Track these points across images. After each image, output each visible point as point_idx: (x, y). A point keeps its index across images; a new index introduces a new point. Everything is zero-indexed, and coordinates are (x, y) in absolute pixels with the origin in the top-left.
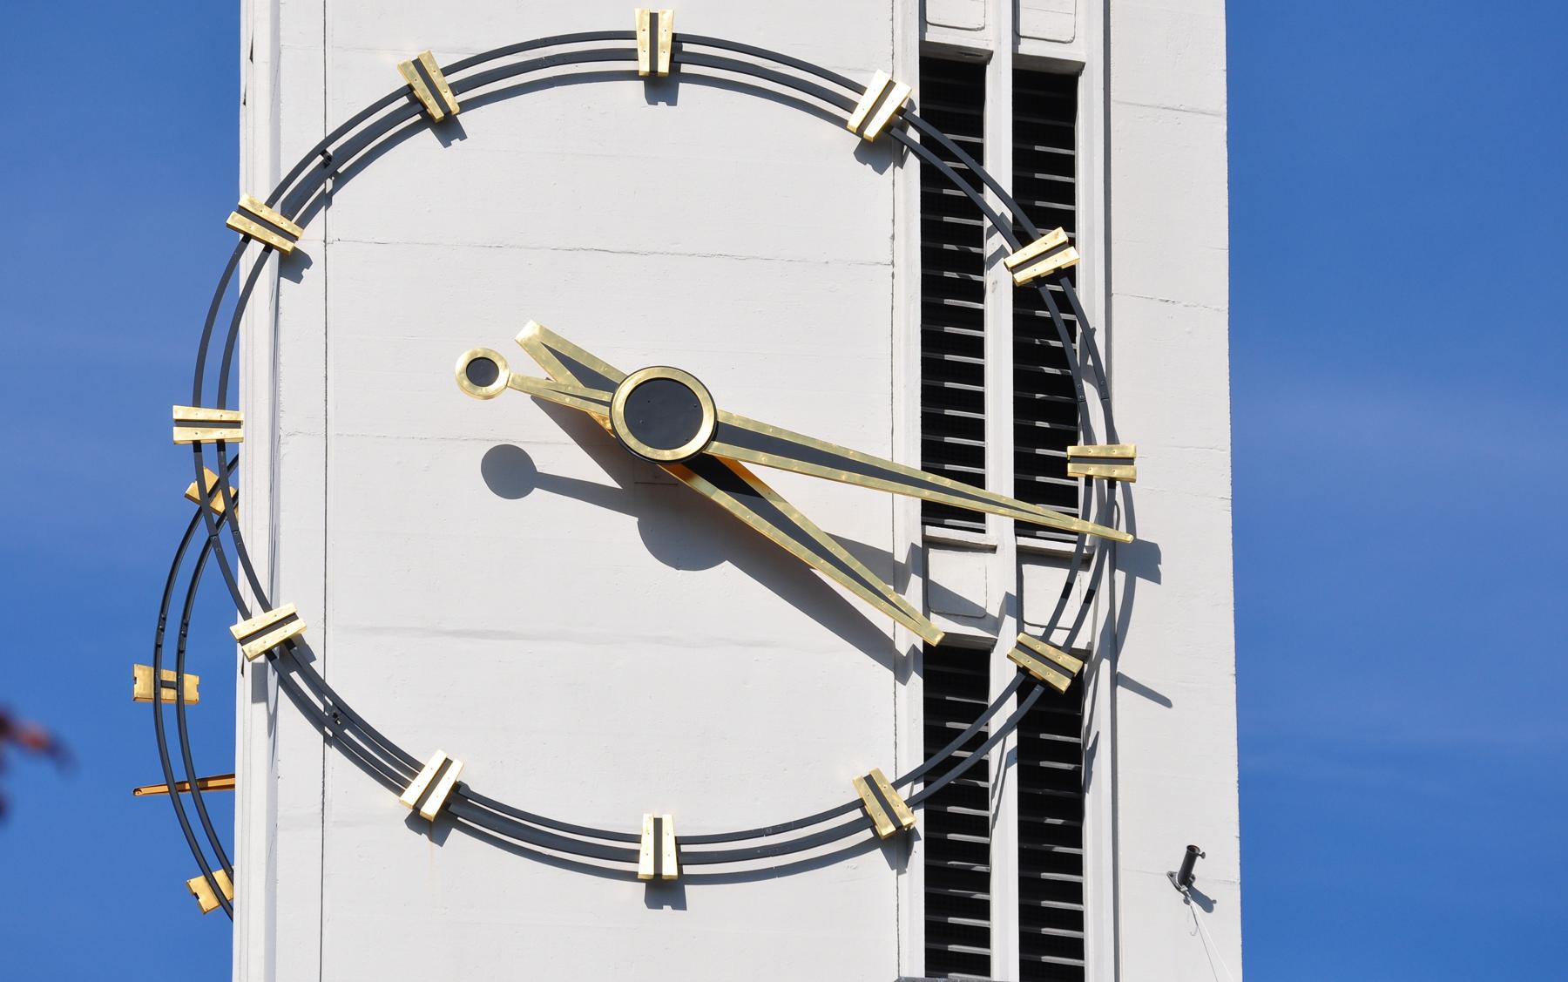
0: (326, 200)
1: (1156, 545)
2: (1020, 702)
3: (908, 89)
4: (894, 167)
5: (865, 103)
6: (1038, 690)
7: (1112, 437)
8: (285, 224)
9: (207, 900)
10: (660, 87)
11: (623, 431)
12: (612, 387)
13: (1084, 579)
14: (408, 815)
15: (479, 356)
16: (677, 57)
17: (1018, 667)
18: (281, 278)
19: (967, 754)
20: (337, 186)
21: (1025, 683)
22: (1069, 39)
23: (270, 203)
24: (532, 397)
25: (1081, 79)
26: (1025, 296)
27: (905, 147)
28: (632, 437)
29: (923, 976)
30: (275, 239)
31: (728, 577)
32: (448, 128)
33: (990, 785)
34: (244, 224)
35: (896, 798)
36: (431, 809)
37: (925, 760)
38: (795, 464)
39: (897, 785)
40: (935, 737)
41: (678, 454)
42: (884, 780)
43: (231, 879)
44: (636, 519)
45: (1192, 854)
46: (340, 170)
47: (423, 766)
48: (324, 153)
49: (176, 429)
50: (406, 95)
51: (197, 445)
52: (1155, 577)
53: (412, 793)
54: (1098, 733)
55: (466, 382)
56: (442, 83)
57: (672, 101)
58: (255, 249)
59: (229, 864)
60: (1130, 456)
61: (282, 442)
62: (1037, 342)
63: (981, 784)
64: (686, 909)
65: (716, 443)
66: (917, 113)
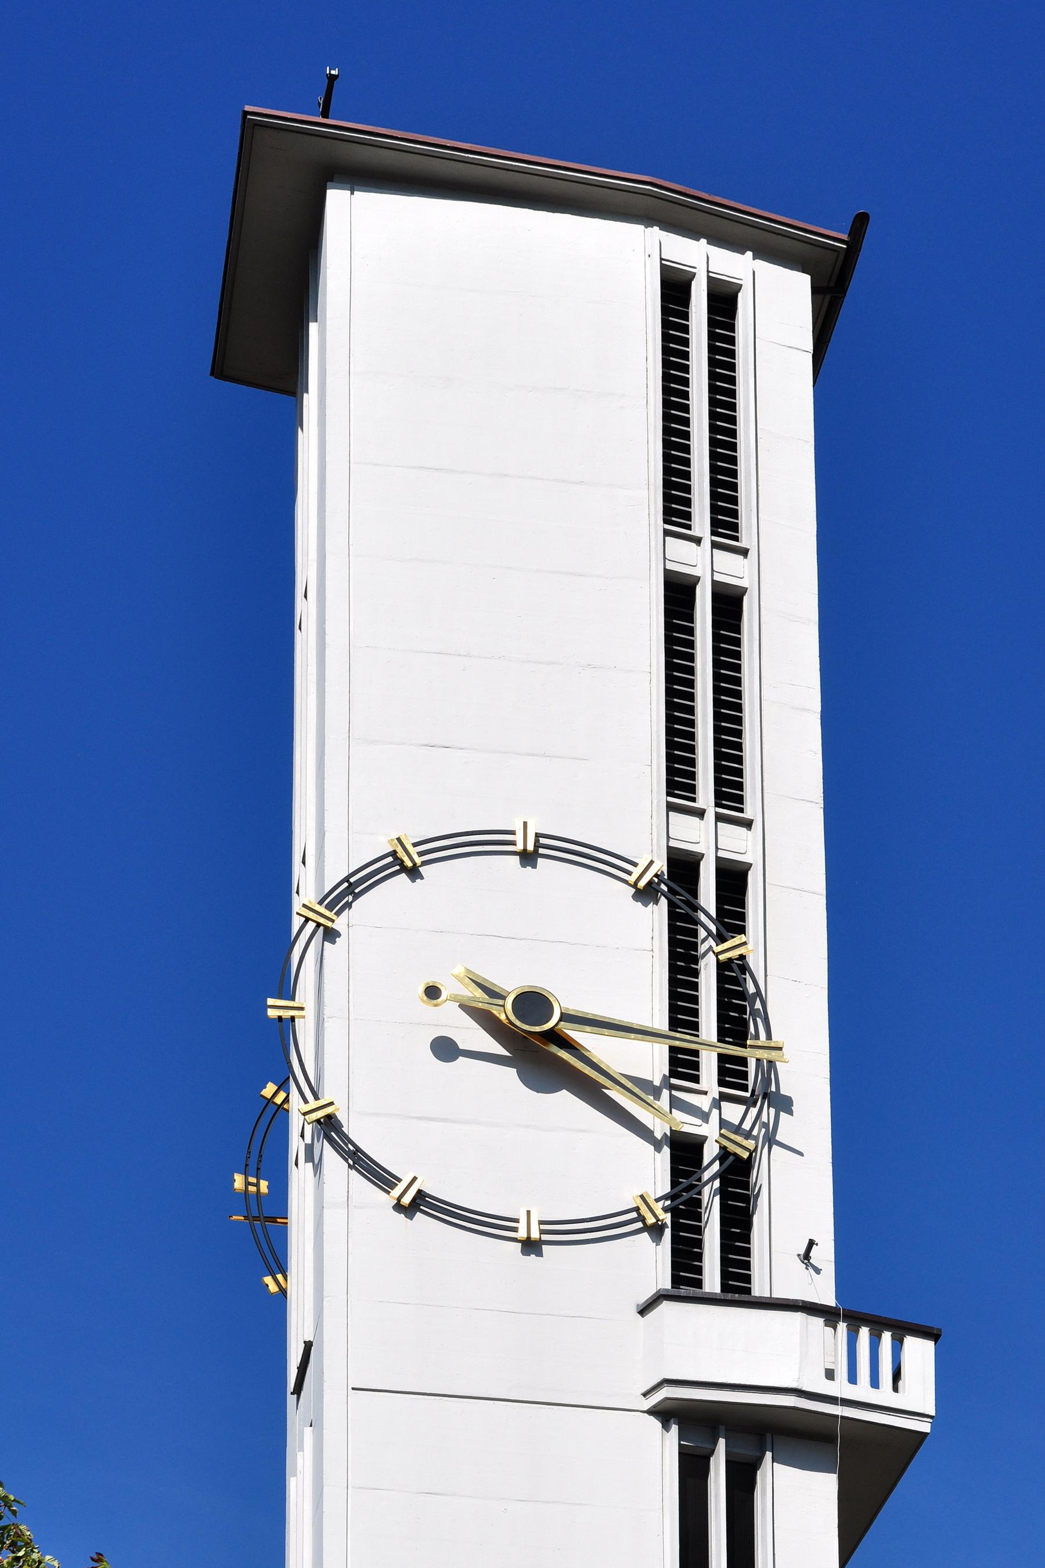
0: (349, 905)
1: (790, 1097)
2: (721, 1165)
3: (661, 865)
4: (653, 904)
5: (637, 872)
6: (732, 1158)
7: (769, 1036)
8: (327, 913)
9: (273, 1288)
10: (528, 858)
11: (513, 1018)
12: (504, 998)
13: (754, 1111)
14: (394, 1204)
15: (431, 985)
16: (538, 844)
17: (720, 1146)
18: (325, 942)
19: (694, 1182)
20: (354, 900)
21: (724, 1155)
22: (744, 852)
23: (321, 903)
24: (459, 1006)
25: (750, 873)
26: (723, 967)
27: (659, 894)
28: (517, 1020)
29: (670, 1287)
30: (322, 920)
31: (565, 1099)
32: (414, 873)
33: (703, 1211)
34: (306, 912)
35: (656, 1207)
36: (406, 1200)
37: (671, 1189)
38: (606, 1031)
39: (657, 1200)
40: (676, 1174)
41: (543, 1028)
42: (649, 1197)
43: (286, 1280)
44: (515, 1070)
45: (811, 1243)
46: (357, 891)
47: (402, 1180)
48: (348, 881)
49: (269, 1010)
50: (392, 856)
51: (280, 1018)
52: (791, 1113)
53: (396, 1192)
54: (761, 1185)
55: (425, 998)
56: (413, 851)
57: (534, 866)
58: (311, 926)
59: (284, 1271)
60: (781, 1046)
61: (325, 1021)
62: (726, 1000)
63: (699, 1210)
64: (542, 1257)
65: (562, 1023)
66: (666, 877)
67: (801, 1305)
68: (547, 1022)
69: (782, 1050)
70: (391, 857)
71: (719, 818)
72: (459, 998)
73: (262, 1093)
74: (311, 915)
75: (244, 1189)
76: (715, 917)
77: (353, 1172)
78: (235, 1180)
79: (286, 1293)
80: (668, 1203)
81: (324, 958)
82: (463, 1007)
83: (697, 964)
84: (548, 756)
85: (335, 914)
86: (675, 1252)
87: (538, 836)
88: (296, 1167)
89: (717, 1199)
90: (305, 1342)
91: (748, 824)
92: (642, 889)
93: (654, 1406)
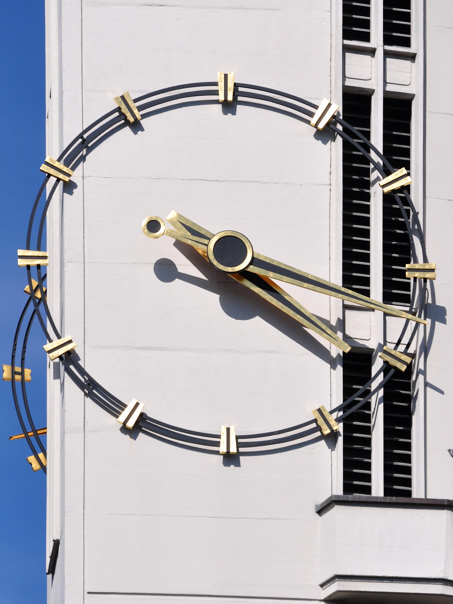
0: (83, 158)
5: (318, 113)
6: (392, 371)
7: (425, 260)
8: (65, 169)
9: (36, 466)
12: (209, 239)
15: (153, 219)
16: (236, 93)
18: (64, 193)
20: (88, 152)
22: (408, 84)
27: (336, 133)
30: (61, 176)
34: (48, 169)
36: (131, 424)
37: (343, 401)
39: (331, 412)
46: (89, 145)
48: (82, 137)
49: (19, 260)
51: (28, 267)
54: (418, 389)
55: (146, 230)
56: (134, 106)
57: (234, 113)
60: (433, 268)
61: (65, 265)
62: (393, 219)
65: (252, 266)
66: (341, 117)
67: (446, 504)
68: (240, 264)
69: (434, 272)
70: (117, 113)
71: (387, 54)
72: (174, 233)
73: (25, 290)
74: (52, 171)
75: (11, 378)
76: (382, 153)
77: (88, 400)
80: (341, 413)
81: (64, 208)
83: (369, 189)
84: (246, 9)
86: (346, 451)
89: (381, 406)
90: (54, 540)
91: (412, 57)
92: (321, 130)
93: (329, 596)
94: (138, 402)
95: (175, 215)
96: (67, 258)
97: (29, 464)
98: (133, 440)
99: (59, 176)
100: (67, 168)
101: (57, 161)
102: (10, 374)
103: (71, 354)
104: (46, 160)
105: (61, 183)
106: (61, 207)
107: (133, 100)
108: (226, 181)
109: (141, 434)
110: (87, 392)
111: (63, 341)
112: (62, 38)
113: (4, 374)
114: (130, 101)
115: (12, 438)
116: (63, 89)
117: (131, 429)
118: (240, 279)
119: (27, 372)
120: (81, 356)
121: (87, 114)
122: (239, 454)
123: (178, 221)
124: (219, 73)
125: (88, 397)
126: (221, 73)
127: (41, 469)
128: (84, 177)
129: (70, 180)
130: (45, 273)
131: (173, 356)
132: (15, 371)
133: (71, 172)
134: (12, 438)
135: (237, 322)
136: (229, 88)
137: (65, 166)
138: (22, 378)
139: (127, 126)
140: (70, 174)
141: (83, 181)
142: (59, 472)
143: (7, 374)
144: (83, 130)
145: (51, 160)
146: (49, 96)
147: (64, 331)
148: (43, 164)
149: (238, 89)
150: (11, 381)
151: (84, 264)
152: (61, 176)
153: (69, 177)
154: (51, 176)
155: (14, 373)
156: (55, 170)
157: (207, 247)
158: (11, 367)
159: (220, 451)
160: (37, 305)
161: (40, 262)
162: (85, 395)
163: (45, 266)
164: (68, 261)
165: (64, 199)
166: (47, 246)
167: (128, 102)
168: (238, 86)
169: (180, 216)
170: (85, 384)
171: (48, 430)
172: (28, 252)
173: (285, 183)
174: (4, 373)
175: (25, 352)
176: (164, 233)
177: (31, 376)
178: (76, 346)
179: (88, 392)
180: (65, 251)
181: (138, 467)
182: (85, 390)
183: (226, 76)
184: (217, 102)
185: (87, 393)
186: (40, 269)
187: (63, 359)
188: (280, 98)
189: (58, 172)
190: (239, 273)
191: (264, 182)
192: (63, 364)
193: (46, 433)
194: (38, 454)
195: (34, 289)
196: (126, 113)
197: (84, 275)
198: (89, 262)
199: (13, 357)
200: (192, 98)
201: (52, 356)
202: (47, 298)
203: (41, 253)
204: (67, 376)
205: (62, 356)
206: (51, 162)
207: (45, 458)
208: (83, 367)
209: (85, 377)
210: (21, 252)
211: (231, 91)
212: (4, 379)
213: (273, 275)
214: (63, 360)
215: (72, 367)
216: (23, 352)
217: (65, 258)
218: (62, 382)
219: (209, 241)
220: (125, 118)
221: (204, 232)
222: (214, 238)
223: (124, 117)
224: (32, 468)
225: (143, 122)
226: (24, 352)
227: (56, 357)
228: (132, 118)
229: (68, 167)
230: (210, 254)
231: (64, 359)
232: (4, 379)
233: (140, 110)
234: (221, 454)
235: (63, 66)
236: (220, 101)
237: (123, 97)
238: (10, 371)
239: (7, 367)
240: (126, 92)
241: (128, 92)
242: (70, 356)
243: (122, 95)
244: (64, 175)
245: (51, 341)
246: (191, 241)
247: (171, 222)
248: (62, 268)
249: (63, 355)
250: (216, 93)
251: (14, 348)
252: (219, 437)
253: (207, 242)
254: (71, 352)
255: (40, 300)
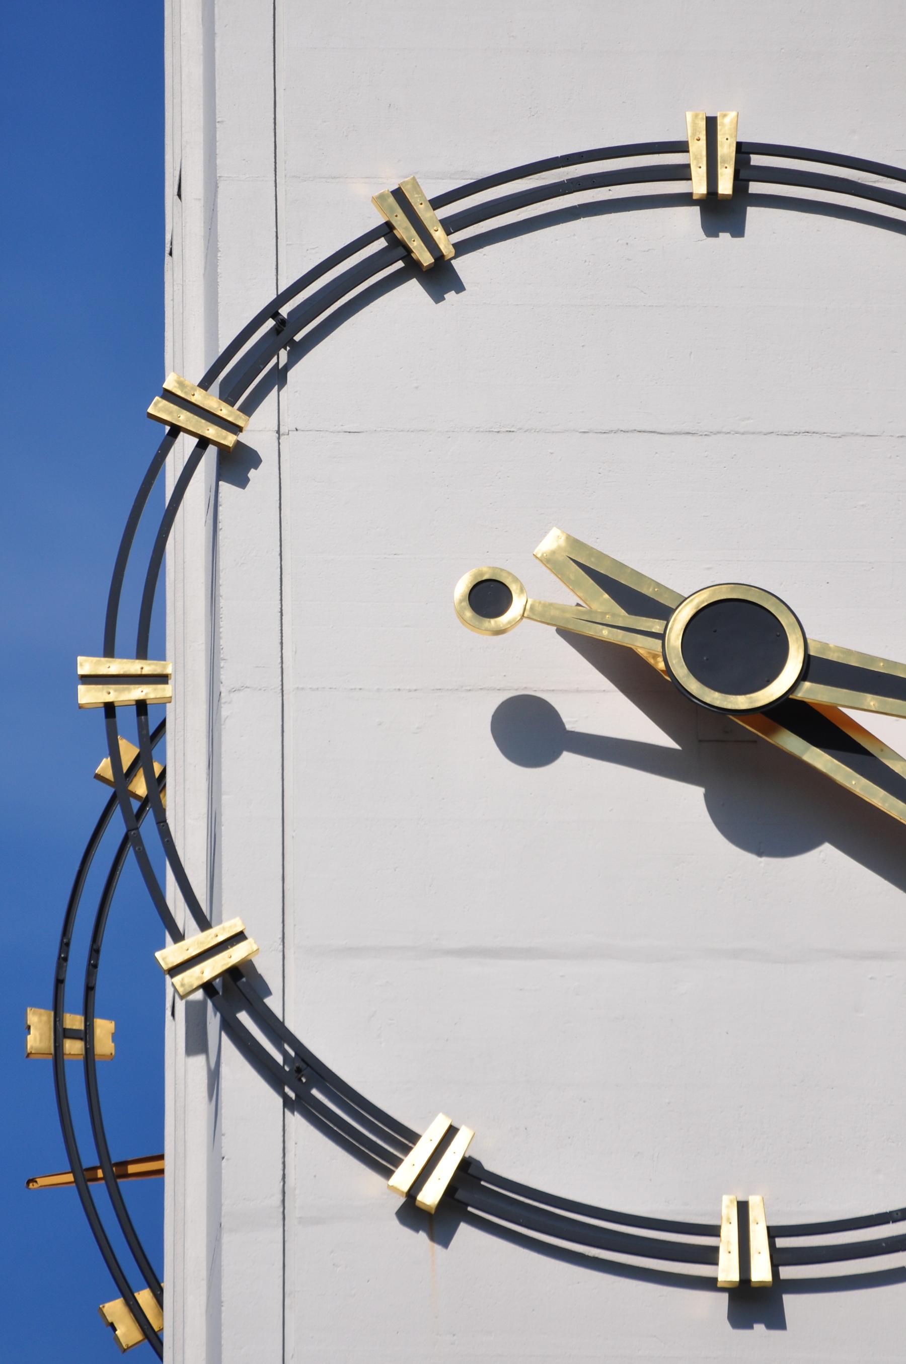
0: (279, 377)
8: (225, 411)
12: (664, 613)
15: (486, 577)
18: (221, 483)
20: (294, 358)
30: (211, 431)
34: (171, 413)
46: (298, 337)
48: (275, 315)
49: (82, 689)
51: (110, 709)
53: (404, 1177)
55: (469, 613)
56: (432, 218)
57: (738, 231)
58: (185, 445)
61: (223, 700)
65: (807, 685)
72: (553, 612)
73: (96, 772)
74: (183, 418)
77: (296, 1121)
78: (29, 1028)
79: (161, 1343)
81: (220, 526)
82: (566, 634)
85: (240, 409)
87: (743, 150)
88: (172, 1018)
94: (453, 1124)
95: (562, 541)
96: (228, 676)
97: (107, 1326)
98: (438, 1248)
99: (207, 432)
100: (230, 408)
101: (198, 388)
102: (50, 1037)
103: (242, 976)
104: (165, 386)
105: (211, 453)
106: (211, 522)
107: (431, 201)
108: (719, 433)
109: (464, 1229)
110: (292, 1095)
111: (217, 936)
112: (216, 27)
113: (29, 1037)
114: (421, 204)
115: (34, 1184)
116: (218, 175)
117: (433, 1212)
118: (770, 732)
119: (104, 1029)
120: (273, 982)
121: (290, 245)
122: (779, 1286)
123: (569, 557)
124: (689, 116)
125: (296, 1113)
126: (696, 116)
127: (146, 1341)
128: (281, 432)
129: (238, 444)
130: (163, 719)
131: (562, 976)
132: (64, 1027)
133: (240, 418)
134: (36, 1182)
135: (762, 865)
136: (721, 157)
137: (224, 401)
138: (86, 1049)
139: (412, 279)
140: (240, 423)
141: (279, 444)
142: (204, 1355)
143: (38, 1039)
144: (279, 293)
145: (181, 384)
146: (176, 193)
147: (221, 905)
148: (157, 398)
149: (749, 160)
150: (51, 1058)
151: (280, 695)
152: (211, 431)
153: (235, 433)
154: (182, 433)
155: (61, 1033)
156: (192, 415)
157: (660, 642)
158: (52, 1013)
159: (719, 1279)
160: (134, 819)
161: (146, 694)
162: (285, 1105)
163: (162, 705)
164: (232, 686)
165: (220, 499)
166: (168, 638)
167: (415, 208)
168: (748, 151)
169: (574, 543)
170: (287, 1069)
171: (168, 1164)
172: (110, 662)
173: (901, 435)
174: (29, 1033)
175: (95, 966)
176: (526, 615)
177: (114, 1040)
178: (258, 949)
179: (296, 1095)
180: (222, 656)
181: (455, 1337)
182: (287, 1090)
183: (711, 124)
184: (686, 199)
185: (294, 1098)
186: (146, 714)
187: (217, 993)
188: (878, 181)
189: (203, 421)
190: (763, 713)
191: (835, 433)
192: (217, 1008)
193: (161, 1172)
194: (136, 1295)
195: (125, 769)
196: (410, 239)
197: (281, 729)
198: (298, 688)
199: (59, 982)
200: (610, 190)
201: (182, 985)
202: (165, 795)
203: (149, 664)
204: (228, 1046)
205: (214, 983)
206: (182, 391)
207: (160, 1308)
208: (279, 1015)
209: (287, 1047)
210: (86, 665)
211: (726, 165)
212: (28, 1055)
213: (876, 705)
214: (217, 996)
215: (244, 1017)
216: (91, 967)
217: (223, 677)
218: (213, 1065)
219: (665, 622)
220: (406, 254)
221: (651, 590)
222: (679, 612)
223: (401, 251)
224: (117, 1339)
225: (463, 266)
226: (92, 967)
227: (194, 987)
228: (428, 254)
229: (233, 405)
230: (674, 662)
231: (221, 994)
232: (31, 1053)
233: (452, 231)
234: (722, 1290)
235: (217, 107)
236: (695, 197)
237: (398, 194)
238: (50, 1028)
239: (40, 1015)
240: (406, 179)
241: (414, 179)
242: (239, 983)
243: (396, 187)
244: (220, 429)
245: (178, 937)
246: (610, 628)
247: (550, 562)
248: (215, 708)
249: (218, 980)
250: (682, 173)
251: (63, 956)
252: (714, 1231)
253: (658, 627)
254: (243, 971)
255: (145, 802)
